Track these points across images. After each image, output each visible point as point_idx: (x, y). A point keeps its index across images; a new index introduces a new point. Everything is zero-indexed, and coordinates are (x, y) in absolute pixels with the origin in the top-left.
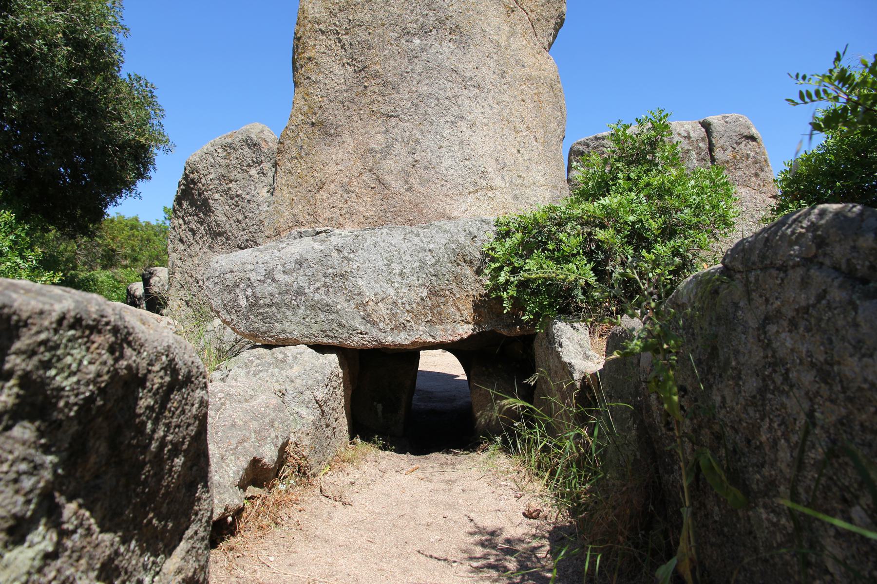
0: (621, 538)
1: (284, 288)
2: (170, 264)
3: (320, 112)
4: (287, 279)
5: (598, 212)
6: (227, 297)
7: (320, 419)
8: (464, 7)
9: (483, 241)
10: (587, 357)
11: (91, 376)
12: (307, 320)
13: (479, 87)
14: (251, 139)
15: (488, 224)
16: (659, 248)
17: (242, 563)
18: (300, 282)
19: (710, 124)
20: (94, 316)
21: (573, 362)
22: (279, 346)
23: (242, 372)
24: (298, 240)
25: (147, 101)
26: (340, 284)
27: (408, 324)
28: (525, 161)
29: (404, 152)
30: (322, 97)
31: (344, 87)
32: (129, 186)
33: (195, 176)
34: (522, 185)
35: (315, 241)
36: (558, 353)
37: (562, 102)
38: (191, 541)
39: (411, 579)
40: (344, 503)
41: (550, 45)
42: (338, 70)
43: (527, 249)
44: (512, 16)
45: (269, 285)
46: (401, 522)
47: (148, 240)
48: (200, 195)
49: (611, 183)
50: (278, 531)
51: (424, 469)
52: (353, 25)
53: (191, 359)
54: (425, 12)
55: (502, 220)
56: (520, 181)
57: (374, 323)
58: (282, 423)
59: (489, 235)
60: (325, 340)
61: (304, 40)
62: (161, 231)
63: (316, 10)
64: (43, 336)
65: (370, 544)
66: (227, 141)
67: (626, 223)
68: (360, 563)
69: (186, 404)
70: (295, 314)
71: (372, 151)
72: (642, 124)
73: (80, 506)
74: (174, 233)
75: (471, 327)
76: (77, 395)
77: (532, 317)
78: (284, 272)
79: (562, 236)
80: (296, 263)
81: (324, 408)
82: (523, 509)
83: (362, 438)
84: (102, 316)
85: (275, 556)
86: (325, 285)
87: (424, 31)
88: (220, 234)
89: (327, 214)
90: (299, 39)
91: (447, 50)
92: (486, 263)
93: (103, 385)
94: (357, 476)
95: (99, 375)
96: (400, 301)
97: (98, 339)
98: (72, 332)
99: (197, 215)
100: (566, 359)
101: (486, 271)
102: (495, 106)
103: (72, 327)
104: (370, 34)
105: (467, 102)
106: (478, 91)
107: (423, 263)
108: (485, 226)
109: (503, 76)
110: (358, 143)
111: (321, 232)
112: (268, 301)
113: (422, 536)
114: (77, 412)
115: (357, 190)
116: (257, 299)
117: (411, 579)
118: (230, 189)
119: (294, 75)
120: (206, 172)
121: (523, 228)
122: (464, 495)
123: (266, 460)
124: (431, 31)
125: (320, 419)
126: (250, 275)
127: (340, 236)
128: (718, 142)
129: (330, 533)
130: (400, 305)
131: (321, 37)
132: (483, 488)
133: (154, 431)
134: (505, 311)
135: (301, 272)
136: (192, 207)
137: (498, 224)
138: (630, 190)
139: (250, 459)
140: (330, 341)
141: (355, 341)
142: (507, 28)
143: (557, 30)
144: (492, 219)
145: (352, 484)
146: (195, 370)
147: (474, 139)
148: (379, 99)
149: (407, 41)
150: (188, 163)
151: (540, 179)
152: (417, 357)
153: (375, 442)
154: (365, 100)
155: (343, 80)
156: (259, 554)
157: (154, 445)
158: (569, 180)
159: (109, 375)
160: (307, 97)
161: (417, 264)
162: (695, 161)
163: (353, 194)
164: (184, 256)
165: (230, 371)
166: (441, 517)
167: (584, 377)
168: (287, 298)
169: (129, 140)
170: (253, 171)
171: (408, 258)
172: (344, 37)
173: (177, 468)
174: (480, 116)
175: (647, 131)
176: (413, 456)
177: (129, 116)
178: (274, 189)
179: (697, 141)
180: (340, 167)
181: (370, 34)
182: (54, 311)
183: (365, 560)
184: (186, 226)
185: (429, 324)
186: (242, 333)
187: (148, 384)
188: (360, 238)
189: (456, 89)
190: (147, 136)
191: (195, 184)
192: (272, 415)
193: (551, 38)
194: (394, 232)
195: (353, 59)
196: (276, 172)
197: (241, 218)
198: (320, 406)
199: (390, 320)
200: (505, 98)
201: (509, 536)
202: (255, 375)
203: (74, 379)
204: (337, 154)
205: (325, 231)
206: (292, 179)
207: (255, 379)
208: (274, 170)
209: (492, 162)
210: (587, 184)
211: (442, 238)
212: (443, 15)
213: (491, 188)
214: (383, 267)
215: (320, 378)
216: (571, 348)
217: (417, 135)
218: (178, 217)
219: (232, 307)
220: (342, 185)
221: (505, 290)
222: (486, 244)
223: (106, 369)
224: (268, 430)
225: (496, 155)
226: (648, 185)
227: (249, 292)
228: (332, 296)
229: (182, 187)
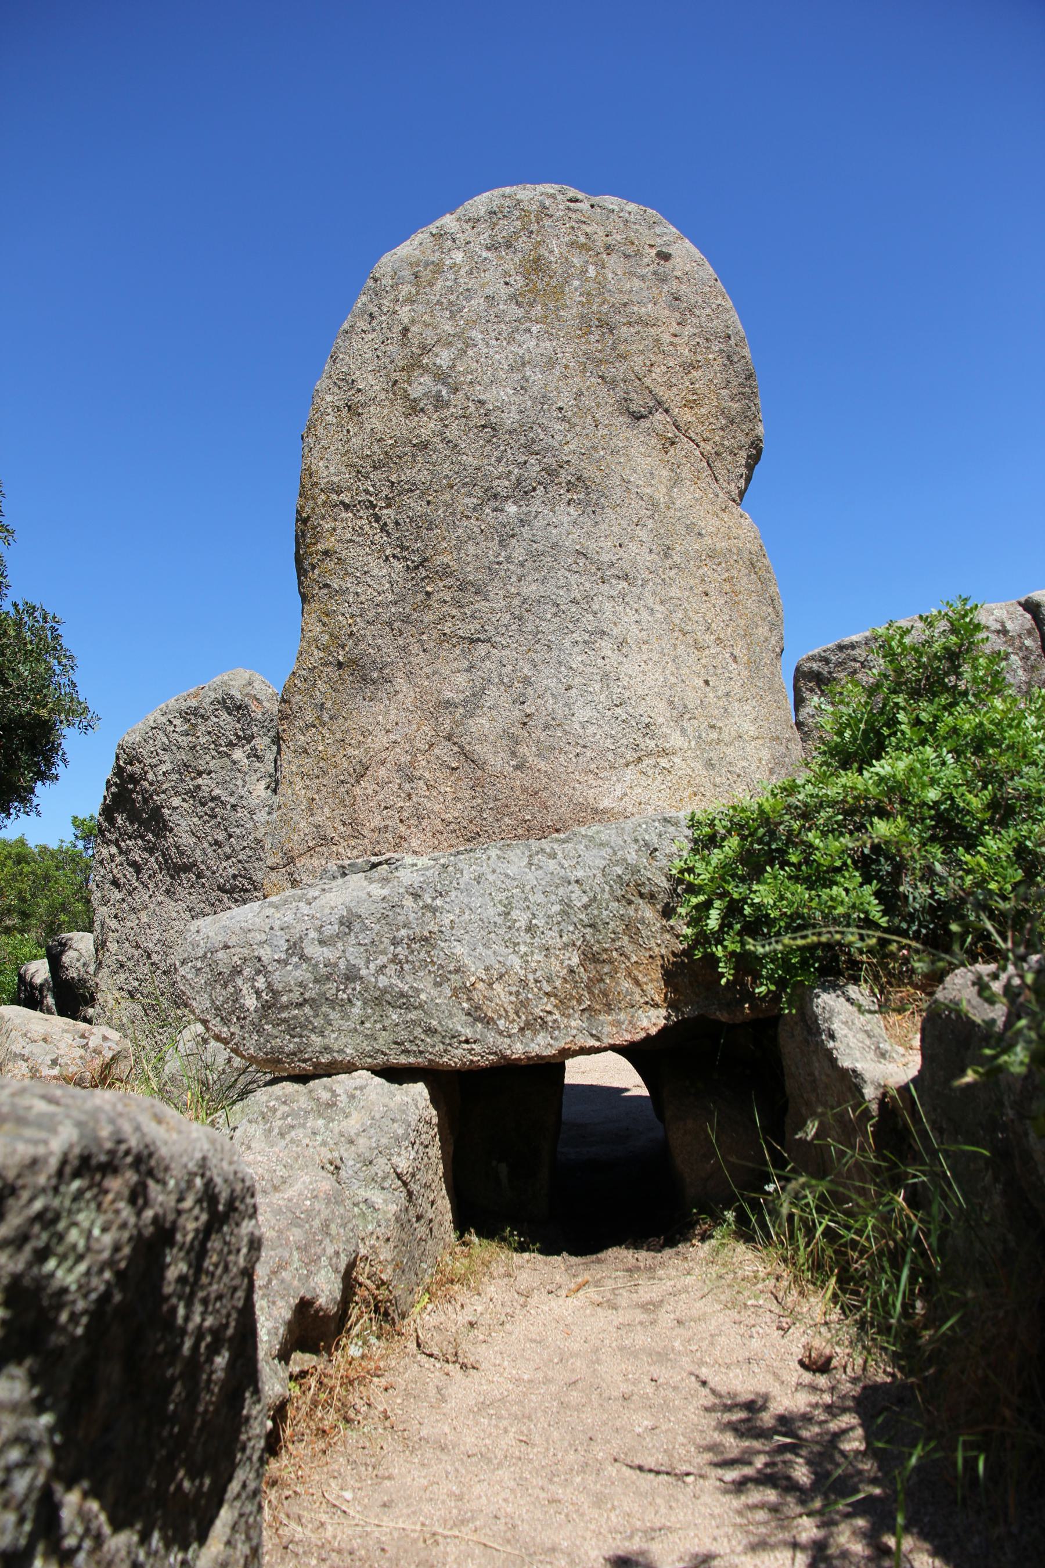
0: (1007, 1413)
1: (323, 971)
2: (97, 926)
3: (350, 643)
5: (874, 791)
6: (221, 994)
7: (407, 1209)
8: (589, 444)
9: (670, 857)
10: (883, 1055)
11: (106, 1255)
12: (368, 1025)
13: (626, 577)
14: (232, 698)
15: (676, 824)
16: (992, 844)
17: (295, 1510)
18: (351, 958)
19: (1038, 605)
20: (108, 1145)
21: (859, 1066)
22: (319, 1076)
23: (256, 1130)
24: (340, 881)
25: (46, 645)
26: (423, 955)
27: (549, 1018)
28: (719, 698)
29: (505, 701)
30: (352, 616)
31: (391, 597)
32: (24, 795)
33: (136, 768)
34: (719, 741)
35: (371, 881)
36: (829, 1052)
37: (774, 589)
38: (238, 1504)
39: (613, 1516)
40: (464, 1366)
41: (742, 494)
42: (376, 568)
43: (753, 864)
44: (672, 451)
45: (296, 966)
46: (575, 1396)
47: (47, 878)
48: (145, 801)
49: (885, 731)
50: (352, 1436)
51: (597, 1284)
52: (398, 491)
53: (232, 1168)
54: (522, 459)
55: (700, 816)
56: (714, 735)
57: (488, 1022)
58: (344, 1225)
59: (677, 846)
60: (403, 1060)
61: (314, 521)
62: (68, 859)
63: (332, 470)
64: (38, 1205)
65: (524, 1447)
66: (189, 703)
67: (924, 804)
68: (513, 1491)
69: (230, 1252)
70: (346, 1016)
71: (448, 704)
72: (931, 625)
73: (85, 1495)
74: (102, 871)
75: (663, 1012)
76: (85, 1296)
77: (773, 988)
78: (322, 942)
79: (811, 836)
80: (342, 923)
81: (414, 1187)
82: (799, 1352)
83: (479, 1235)
84: (119, 1142)
85: (353, 1489)
87: (523, 491)
88: (186, 868)
89: (377, 821)
90: (305, 521)
91: (566, 519)
92: (678, 895)
93: (123, 1265)
94: (480, 1309)
95: (117, 1248)
96: (531, 977)
97: (115, 1184)
98: (76, 1184)
99: (142, 837)
100: (845, 1063)
101: (682, 911)
102: (657, 607)
103: (77, 1174)
104: (429, 503)
105: (608, 606)
106: (625, 584)
107: (567, 906)
108: (672, 829)
109: (667, 556)
111: (380, 864)
112: (296, 997)
113: (618, 1424)
114: (87, 1327)
115: (427, 775)
116: (275, 994)
117: (613, 1516)
118: (199, 787)
119: (300, 583)
120: (154, 761)
121: (737, 827)
122: (680, 1331)
123: (322, 1301)
124: (534, 489)
125: (407, 1209)
126: (261, 952)
127: (415, 867)
129: (447, 1429)
130: (532, 984)
131: (344, 515)
132: (720, 1319)
133: (187, 1318)
134: (723, 981)
135: (352, 939)
136: (132, 823)
137: (694, 823)
138: (923, 742)
139: (294, 1301)
140: (412, 1060)
141: (457, 1057)
142: (665, 473)
143: (750, 467)
144: (683, 815)
145: (472, 1324)
146: (239, 1187)
147: (628, 668)
148: (454, 612)
149: (495, 510)
150: (121, 747)
151: (749, 728)
152: (562, 1068)
153: (504, 1239)
154: (429, 617)
155: (388, 585)
156: (325, 1488)
157: (188, 1344)
158: (799, 725)
159: (132, 1244)
160: (325, 619)
161: (557, 908)
162: (1020, 672)
163: (421, 783)
164: (123, 910)
165: (235, 1129)
166: (647, 1380)
167: (884, 1095)
168: (330, 989)
169: (21, 715)
170: (238, 754)
171: (539, 898)
172: (385, 511)
173: (219, 1375)
174: (634, 628)
175: (941, 639)
176: (573, 1260)
177: (20, 675)
178: (277, 782)
179: (1019, 636)
180: (393, 737)
181: (429, 503)
182: (51, 1154)
183: (521, 1483)
184: (123, 858)
185: (586, 1014)
186: (252, 1059)
187: (179, 1237)
188: (451, 869)
189: (587, 585)
190: (50, 705)
191: (136, 782)
192: (325, 1213)
193: (743, 481)
194: (510, 855)
195: (404, 548)
196: (279, 752)
197: (221, 837)
198: (405, 1184)
199: (517, 1013)
200: (674, 592)
201: (781, 1410)
202: (282, 1135)
203: (82, 1267)
204: (387, 713)
206: (308, 763)
207: (283, 1143)
208: (275, 748)
209: (662, 706)
210: (840, 733)
211: (596, 859)
212: (552, 461)
213: (665, 752)
214: (497, 919)
215: (401, 1131)
216: (852, 1041)
217: (525, 671)
218: (108, 843)
219: (230, 1011)
220: (399, 768)
221: (720, 942)
222: (677, 862)
223: (126, 1235)
224: (321, 1242)
225: (668, 693)
226: (955, 731)
227: (261, 983)
228: (409, 978)
229: (114, 789)
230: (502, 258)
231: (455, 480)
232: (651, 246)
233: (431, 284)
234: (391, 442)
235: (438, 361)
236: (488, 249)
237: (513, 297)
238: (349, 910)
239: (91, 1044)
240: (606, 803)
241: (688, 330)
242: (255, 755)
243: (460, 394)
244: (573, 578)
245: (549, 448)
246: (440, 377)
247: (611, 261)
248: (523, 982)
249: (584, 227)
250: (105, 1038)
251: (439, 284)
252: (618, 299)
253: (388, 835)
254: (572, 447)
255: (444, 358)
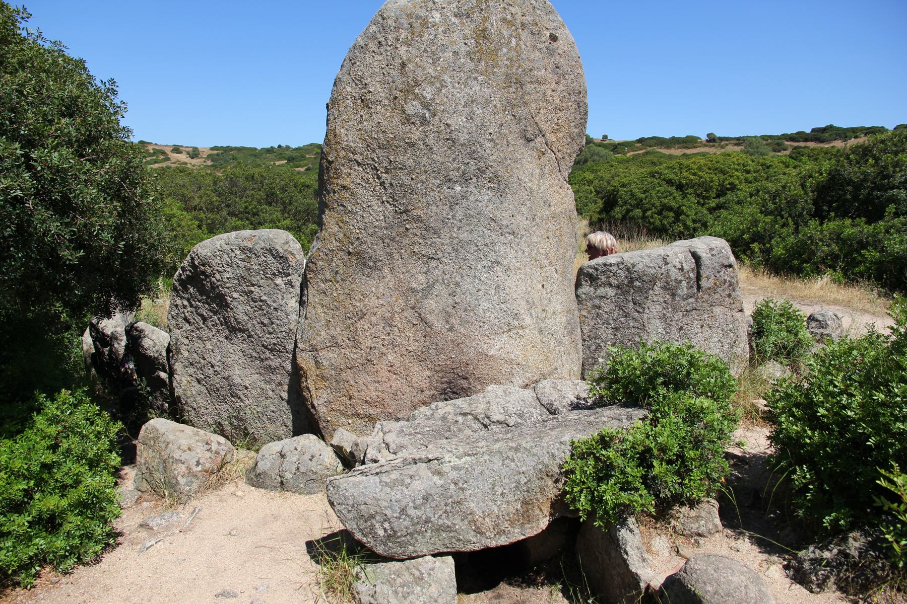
1: (416, 520)
4: (419, 513)
29: (445, 293)
31: (384, 224)
45: (405, 520)
48: (213, 288)
57: (482, 533)
60: (445, 550)
70: (424, 537)
71: (414, 290)
78: (415, 508)
86: (446, 512)
87: (465, 179)
91: (486, 197)
105: (503, 248)
106: (512, 237)
109: (534, 220)
110: (400, 281)
112: (404, 533)
115: (399, 325)
116: (395, 532)
118: (252, 292)
120: (221, 269)
128: (704, 273)
131: (356, 167)
148: (421, 241)
151: (559, 307)
154: (406, 241)
158: (577, 296)
160: (341, 225)
161: (514, 485)
163: (396, 329)
168: (418, 527)
170: (279, 281)
172: (384, 175)
174: (514, 261)
176: (489, 594)
195: (394, 199)
197: (266, 321)
200: (535, 239)
202: (405, 598)
204: (377, 288)
205: (437, 459)
209: (524, 303)
211: (531, 462)
212: (483, 165)
213: (522, 327)
230: (463, 24)
231: (429, 168)
232: (547, 29)
233: (421, 36)
234: (391, 136)
235: (425, 94)
236: (456, 16)
237: (469, 54)
238: (427, 492)
239: (213, 449)
240: (492, 352)
241: (561, 87)
242: (290, 284)
243: (437, 118)
244: (487, 232)
245: (482, 157)
246: (425, 105)
247: (524, 34)
248: (498, 517)
249: (511, 8)
250: (219, 443)
251: (426, 37)
252: (526, 65)
253: (376, 352)
254: (494, 157)
255: (428, 92)
